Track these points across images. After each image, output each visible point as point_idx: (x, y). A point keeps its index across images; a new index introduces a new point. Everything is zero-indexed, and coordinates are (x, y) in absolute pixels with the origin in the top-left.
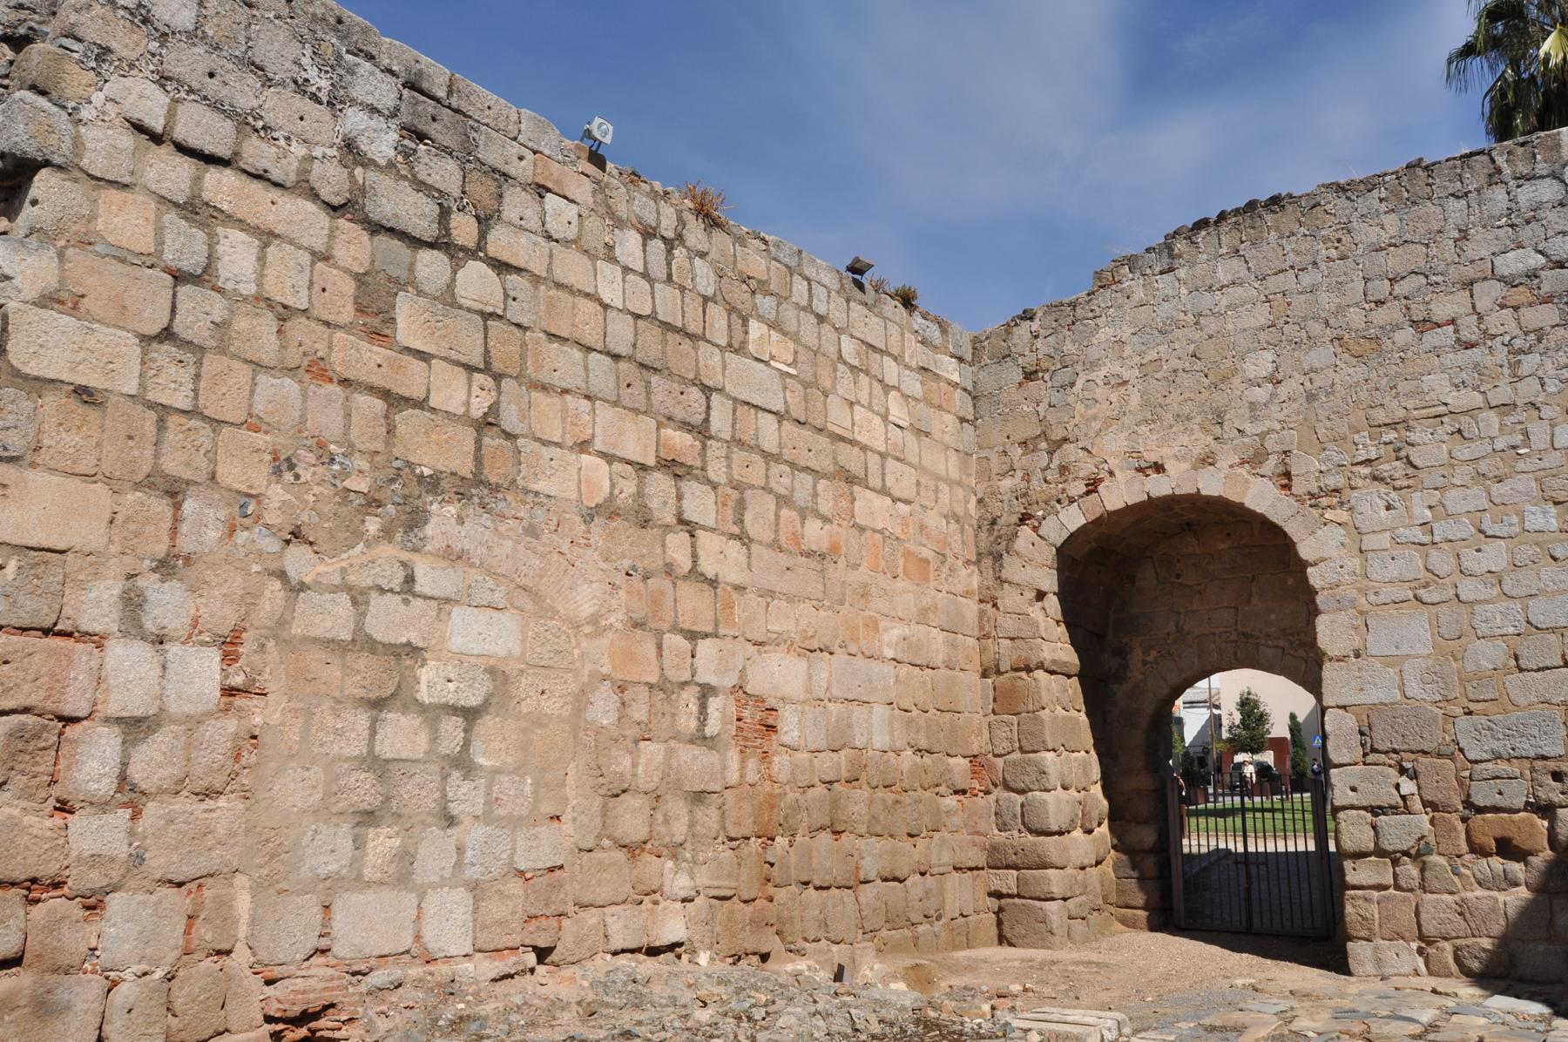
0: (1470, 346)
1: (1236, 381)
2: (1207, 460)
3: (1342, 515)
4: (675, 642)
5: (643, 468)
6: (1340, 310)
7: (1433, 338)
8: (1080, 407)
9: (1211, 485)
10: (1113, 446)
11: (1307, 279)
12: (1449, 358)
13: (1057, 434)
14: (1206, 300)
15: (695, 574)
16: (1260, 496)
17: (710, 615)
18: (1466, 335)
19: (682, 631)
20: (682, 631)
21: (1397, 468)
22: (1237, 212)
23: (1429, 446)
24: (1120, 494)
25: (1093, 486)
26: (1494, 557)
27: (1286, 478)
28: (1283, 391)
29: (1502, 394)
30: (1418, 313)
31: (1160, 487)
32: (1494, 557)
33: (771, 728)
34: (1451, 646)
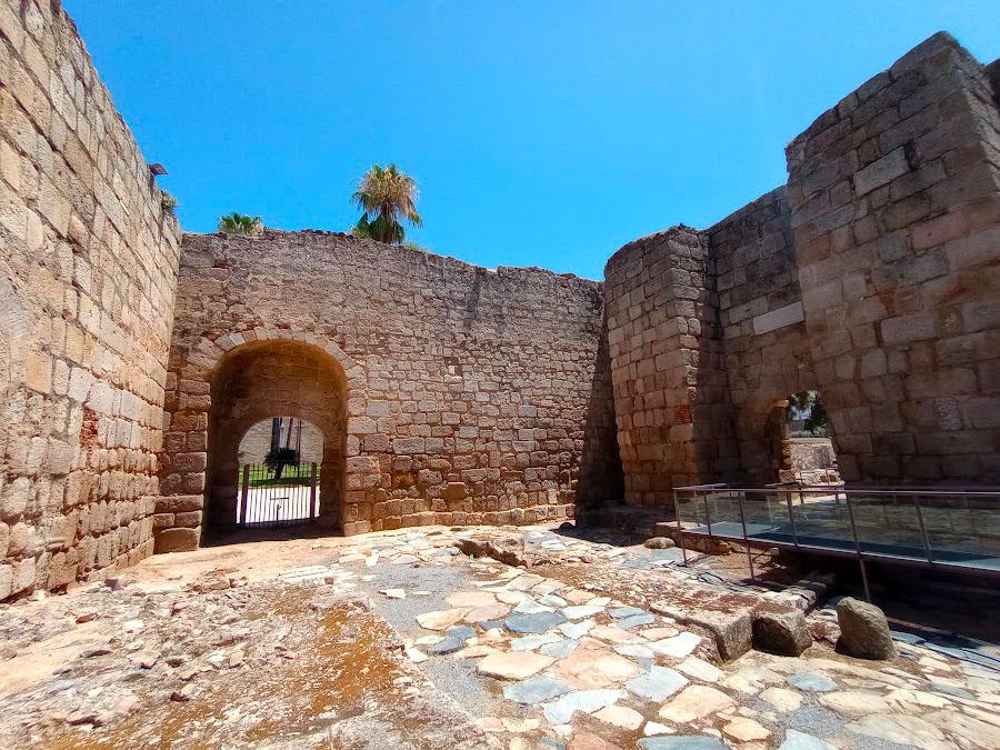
0: (412, 315)
1: (327, 301)
2: (311, 329)
3: (363, 363)
4: (61, 364)
5: (60, 236)
6: (371, 287)
7: (401, 308)
8: (248, 289)
9: (311, 339)
10: (264, 314)
11: (360, 272)
12: (405, 317)
13: (234, 298)
14: (318, 265)
15: (77, 322)
16: (331, 348)
17: (79, 352)
18: (410, 310)
19: (66, 359)
20: (66, 359)
21: (382, 347)
22: (335, 235)
23: (394, 344)
24: (263, 334)
25: (251, 326)
26: (410, 386)
27: (342, 345)
28: (346, 310)
29: (418, 333)
30: (397, 298)
31: (285, 335)
32: (410, 386)
33: (95, 432)
34: (395, 414)
